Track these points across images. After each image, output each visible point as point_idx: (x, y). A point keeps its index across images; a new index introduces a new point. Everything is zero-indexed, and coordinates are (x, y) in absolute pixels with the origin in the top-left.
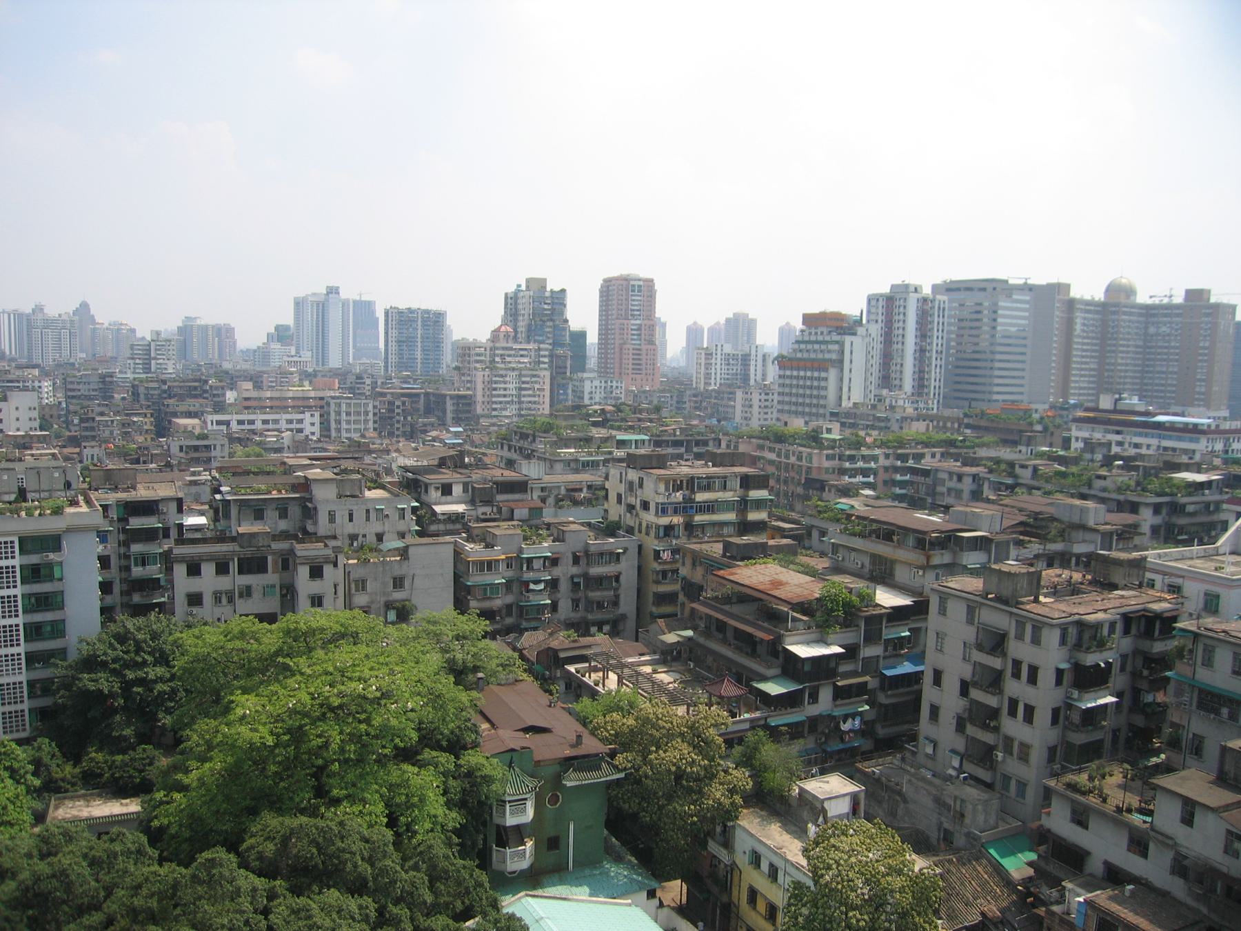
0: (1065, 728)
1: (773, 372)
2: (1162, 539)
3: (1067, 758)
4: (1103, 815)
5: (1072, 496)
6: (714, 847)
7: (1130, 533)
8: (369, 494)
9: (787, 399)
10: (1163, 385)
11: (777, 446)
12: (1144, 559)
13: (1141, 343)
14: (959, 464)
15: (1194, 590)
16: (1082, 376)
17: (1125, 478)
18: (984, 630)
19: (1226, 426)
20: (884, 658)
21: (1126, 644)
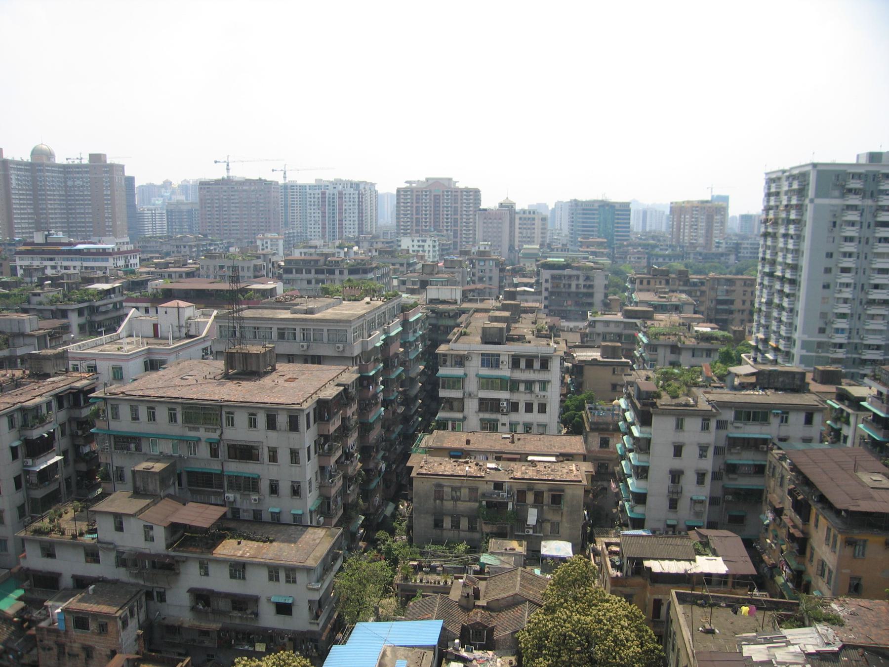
0: (28, 489)
2: (88, 333)
3: (34, 511)
4: (62, 544)
5: (17, 311)
7: (58, 333)
10: (83, 222)
12: (66, 351)
13: (63, 193)
16: (22, 219)
17: (55, 293)
19: (124, 248)
21: (62, 416)
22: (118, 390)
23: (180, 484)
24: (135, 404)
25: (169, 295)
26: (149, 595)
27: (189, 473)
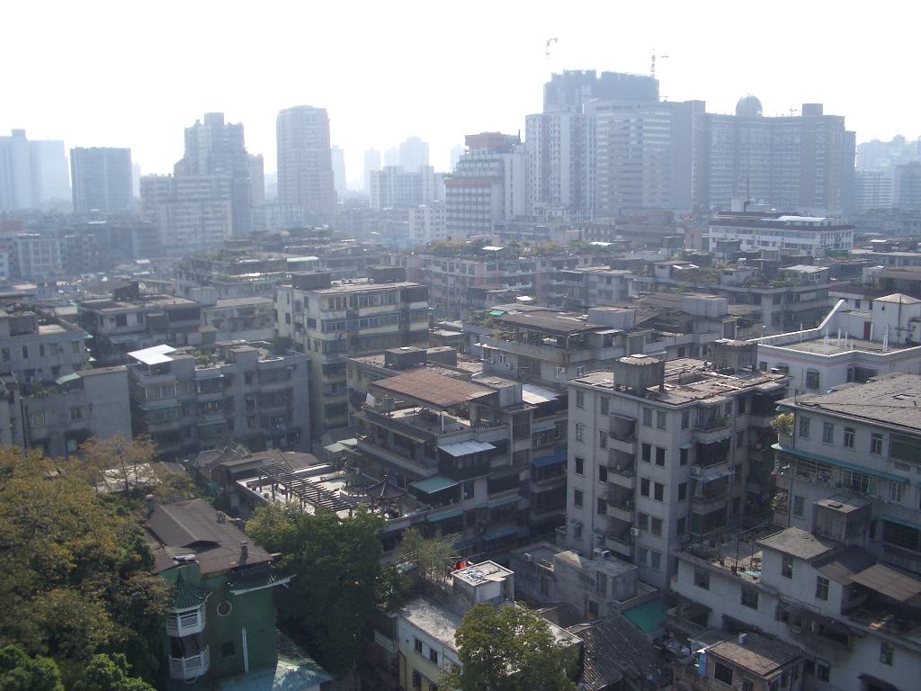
1: (444, 190)
2: (782, 326)
6: (380, 638)
8: (43, 329)
9: (455, 215)
11: (442, 260)
14: (608, 268)
15: (799, 371)
18: (618, 418)
20: (534, 451)
21: (742, 422)
22: (812, 401)
23: (872, 536)
24: (830, 421)
25: (889, 286)
26: (809, 666)
27: (887, 523)
